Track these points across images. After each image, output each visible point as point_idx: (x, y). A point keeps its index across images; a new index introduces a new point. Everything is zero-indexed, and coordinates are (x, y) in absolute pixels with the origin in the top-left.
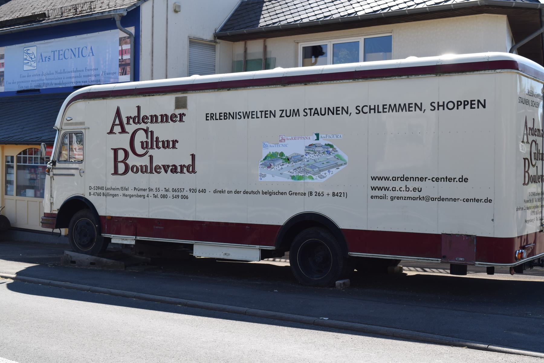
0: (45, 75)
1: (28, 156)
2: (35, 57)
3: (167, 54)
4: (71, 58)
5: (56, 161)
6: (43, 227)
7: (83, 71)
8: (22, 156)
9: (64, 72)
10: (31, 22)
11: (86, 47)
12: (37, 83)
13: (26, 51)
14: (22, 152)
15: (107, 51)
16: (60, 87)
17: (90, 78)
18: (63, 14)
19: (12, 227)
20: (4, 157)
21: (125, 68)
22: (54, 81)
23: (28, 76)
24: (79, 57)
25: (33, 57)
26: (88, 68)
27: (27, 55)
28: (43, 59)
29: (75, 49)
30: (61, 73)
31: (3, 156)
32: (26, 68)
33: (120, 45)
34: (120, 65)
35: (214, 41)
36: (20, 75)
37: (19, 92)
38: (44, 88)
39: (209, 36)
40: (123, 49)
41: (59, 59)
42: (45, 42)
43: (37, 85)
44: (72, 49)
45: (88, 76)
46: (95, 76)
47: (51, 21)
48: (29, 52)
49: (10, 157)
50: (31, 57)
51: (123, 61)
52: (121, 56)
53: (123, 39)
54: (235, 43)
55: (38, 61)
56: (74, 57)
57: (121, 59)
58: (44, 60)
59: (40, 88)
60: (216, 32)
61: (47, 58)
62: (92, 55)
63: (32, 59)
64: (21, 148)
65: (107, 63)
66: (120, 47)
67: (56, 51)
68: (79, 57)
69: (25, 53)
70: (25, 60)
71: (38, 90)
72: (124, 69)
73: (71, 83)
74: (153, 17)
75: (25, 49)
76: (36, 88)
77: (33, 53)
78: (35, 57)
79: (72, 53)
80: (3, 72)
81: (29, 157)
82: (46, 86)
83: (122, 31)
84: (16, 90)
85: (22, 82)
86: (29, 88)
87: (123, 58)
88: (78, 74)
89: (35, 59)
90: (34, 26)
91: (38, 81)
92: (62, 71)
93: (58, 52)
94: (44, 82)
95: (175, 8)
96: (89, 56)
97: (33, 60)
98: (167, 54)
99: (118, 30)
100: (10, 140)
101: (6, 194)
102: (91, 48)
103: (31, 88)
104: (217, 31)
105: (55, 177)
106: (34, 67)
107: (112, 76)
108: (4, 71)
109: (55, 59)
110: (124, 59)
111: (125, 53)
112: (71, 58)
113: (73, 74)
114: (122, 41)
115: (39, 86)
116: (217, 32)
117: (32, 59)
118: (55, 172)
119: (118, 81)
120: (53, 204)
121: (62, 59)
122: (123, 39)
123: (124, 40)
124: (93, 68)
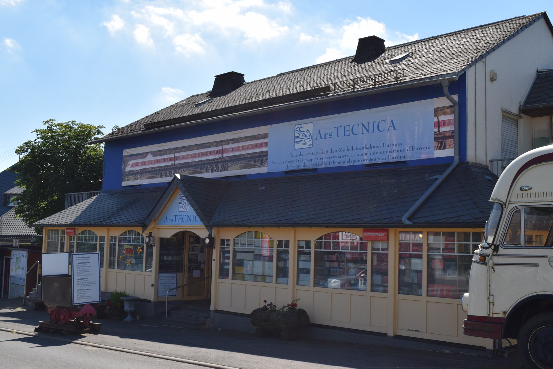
0: (324, 153)
1: (332, 241)
2: (310, 135)
3: (486, 127)
4: (362, 133)
5: (498, 245)
6: (466, 334)
7: (380, 147)
8: (323, 240)
9: (352, 149)
10: (313, 96)
11: (385, 121)
12: (313, 162)
13: (299, 128)
14: (323, 236)
15: (416, 123)
16: (346, 165)
17: (390, 154)
18: (355, 86)
19: (311, 323)
20: (297, 242)
21: (443, 141)
22: (336, 160)
23: (301, 155)
24: (373, 132)
25: (308, 134)
26: (387, 143)
27: (299, 132)
28: (322, 136)
29: (369, 123)
30: (347, 150)
31: (296, 240)
32: (297, 146)
33: (435, 116)
34: (435, 139)
35: (519, 115)
36: (290, 154)
37: (287, 172)
38: (323, 167)
39: (515, 110)
40: (175, 156)
41: (345, 135)
42: (324, 118)
43: (312, 164)
44: (364, 124)
45: (388, 152)
46: (398, 152)
47: (343, 93)
48: (301, 129)
49: (305, 241)
50: (305, 135)
51: (175, 165)
52: (437, 128)
53: (240, 139)
54: (534, 118)
55: (315, 138)
56: (367, 132)
57: (437, 132)
58: (323, 137)
59: (317, 167)
60: (520, 106)
61: (328, 135)
62: (320, 138)
63: (306, 136)
64: (323, 232)
65: (416, 137)
66: (436, 118)
67: (341, 127)
68: (373, 132)
69: (296, 130)
70: (296, 138)
71: (315, 170)
72: (442, 143)
73: (362, 161)
74: (475, 85)
75: (297, 127)
76: (312, 167)
77: (308, 130)
78: (310, 135)
79: (364, 128)
80: (266, 152)
81: (333, 242)
82: (326, 165)
83: (449, 100)
84: (284, 171)
85: (293, 161)
86: (302, 168)
87: (223, 156)
88: (372, 150)
89: (310, 136)
90: (319, 99)
91: (314, 159)
92: (349, 148)
93: (343, 128)
94: (323, 160)
95: (492, 76)
96: (388, 130)
97: (308, 137)
98: (486, 127)
99: (445, 98)
100: (267, 223)
101: (298, 284)
102: (392, 121)
103: (304, 168)
104: (521, 105)
105: (496, 267)
106: (309, 145)
107: (423, 151)
108: (267, 151)
109: (326, 138)
110: (441, 132)
111: (225, 152)
112: (362, 133)
113: (394, 148)
114: (437, 112)
115: (316, 165)
116: (522, 106)
117: (306, 136)
118: (496, 260)
119: (433, 156)
120: (493, 304)
121: (349, 135)
122: (240, 139)
123: (441, 110)
124: (395, 143)
